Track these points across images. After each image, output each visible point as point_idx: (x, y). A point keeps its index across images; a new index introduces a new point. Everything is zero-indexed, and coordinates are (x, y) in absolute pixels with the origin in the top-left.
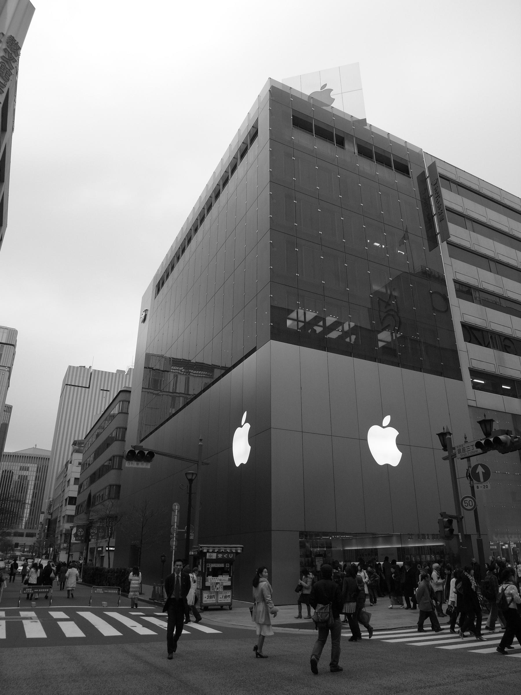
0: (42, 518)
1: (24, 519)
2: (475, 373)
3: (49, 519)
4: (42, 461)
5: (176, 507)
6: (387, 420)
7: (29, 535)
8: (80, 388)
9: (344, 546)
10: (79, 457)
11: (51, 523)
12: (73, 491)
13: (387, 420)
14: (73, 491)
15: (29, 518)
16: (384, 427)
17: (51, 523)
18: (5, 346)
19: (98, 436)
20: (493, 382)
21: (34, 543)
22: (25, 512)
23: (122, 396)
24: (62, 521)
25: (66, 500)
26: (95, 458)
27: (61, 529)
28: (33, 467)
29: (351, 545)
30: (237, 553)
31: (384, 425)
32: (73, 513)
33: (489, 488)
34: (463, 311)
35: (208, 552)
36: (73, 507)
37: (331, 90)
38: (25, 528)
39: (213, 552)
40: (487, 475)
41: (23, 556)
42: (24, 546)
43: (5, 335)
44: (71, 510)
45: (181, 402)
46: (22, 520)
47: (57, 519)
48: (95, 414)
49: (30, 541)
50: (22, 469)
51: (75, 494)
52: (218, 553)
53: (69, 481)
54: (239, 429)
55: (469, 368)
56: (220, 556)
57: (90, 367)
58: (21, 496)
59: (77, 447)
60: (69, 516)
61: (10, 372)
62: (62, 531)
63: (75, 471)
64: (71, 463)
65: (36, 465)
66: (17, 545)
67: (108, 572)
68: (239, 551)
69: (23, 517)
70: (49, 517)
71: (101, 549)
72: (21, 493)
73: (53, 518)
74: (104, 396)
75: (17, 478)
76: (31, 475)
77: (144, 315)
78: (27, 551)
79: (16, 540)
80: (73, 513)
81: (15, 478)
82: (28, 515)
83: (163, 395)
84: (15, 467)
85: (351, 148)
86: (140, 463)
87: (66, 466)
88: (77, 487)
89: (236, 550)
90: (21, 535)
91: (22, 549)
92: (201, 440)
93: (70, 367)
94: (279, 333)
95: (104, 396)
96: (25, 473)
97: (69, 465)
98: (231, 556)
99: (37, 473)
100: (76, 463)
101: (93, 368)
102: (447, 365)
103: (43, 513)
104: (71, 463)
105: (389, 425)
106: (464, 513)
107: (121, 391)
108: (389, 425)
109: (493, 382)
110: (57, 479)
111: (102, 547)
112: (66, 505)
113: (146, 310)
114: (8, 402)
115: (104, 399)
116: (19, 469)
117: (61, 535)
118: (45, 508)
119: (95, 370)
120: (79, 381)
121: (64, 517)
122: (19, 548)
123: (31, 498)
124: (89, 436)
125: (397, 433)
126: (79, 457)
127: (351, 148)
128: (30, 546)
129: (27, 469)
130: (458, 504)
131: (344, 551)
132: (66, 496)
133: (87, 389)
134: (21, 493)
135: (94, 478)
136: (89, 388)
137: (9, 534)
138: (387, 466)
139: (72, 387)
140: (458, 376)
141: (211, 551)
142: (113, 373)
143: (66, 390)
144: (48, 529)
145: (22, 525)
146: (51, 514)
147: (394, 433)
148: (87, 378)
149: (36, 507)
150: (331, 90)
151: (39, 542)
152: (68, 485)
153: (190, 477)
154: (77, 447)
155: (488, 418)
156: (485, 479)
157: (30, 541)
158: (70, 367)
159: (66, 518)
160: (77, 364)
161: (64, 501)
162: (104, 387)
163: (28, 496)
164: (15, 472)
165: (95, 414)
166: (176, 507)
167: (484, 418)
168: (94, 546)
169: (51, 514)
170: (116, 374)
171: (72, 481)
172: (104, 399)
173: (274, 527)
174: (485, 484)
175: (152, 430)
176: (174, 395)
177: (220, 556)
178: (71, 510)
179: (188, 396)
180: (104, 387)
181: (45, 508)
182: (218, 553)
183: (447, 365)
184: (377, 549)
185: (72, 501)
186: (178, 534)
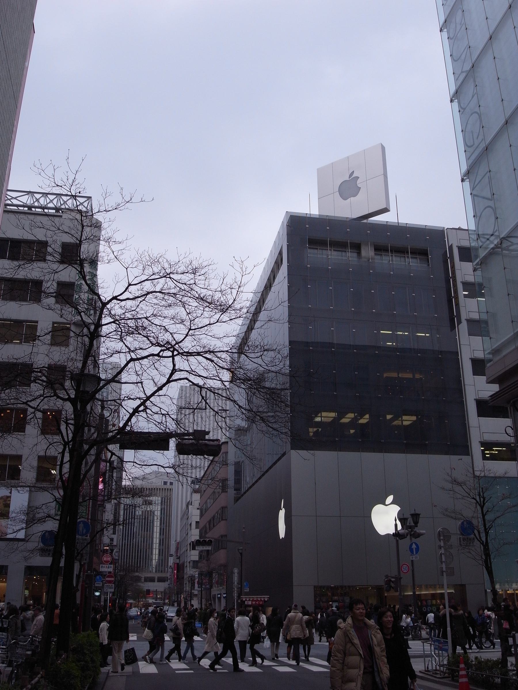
0: (171, 561)
1: (154, 561)
2: (487, 445)
3: (178, 564)
5: (236, 571)
7: (161, 580)
10: (197, 497)
11: (180, 567)
15: (159, 560)
16: (387, 505)
17: (180, 567)
21: (165, 590)
29: (408, 592)
30: (265, 601)
32: (196, 558)
35: (246, 600)
37: (358, 178)
38: (156, 572)
39: (249, 600)
40: (417, 549)
41: (154, 603)
49: (161, 587)
58: (147, 534)
60: (194, 561)
63: (195, 515)
64: (191, 505)
66: (148, 592)
69: (152, 560)
70: (178, 561)
71: (219, 596)
72: (147, 531)
73: (181, 562)
80: (196, 558)
82: (157, 556)
85: (368, 252)
86: (204, 547)
89: (264, 599)
90: (152, 580)
94: (300, 442)
97: (190, 507)
99: (162, 505)
103: (171, 555)
104: (191, 505)
106: (402, 575)
110: (181, 519)
112: (190, 550)
118: (173, 550)
121: (189, 562)
124: (208, 473)
127: (368, 252)
128: (162, 592)
129: (150, 503)
132: (189, 541)
134: (147, 531)
135: (212, 523)
137: (138, 579)
141: (248, 600)
146: (179, 558)
147: (396, 509)
149: (165, 547)
150: (358, 178)
152: (191, 529)
153: (240, 551)
155: (417, 512)
156: (416, 553)
157: (161, 587)
159: (191, 564)
163: (155, 534)
166: (236, 571)
169: (179, 558)
173: (294, 584)
175: (276, 458)
177: (254, 603)
181: (173, 550)
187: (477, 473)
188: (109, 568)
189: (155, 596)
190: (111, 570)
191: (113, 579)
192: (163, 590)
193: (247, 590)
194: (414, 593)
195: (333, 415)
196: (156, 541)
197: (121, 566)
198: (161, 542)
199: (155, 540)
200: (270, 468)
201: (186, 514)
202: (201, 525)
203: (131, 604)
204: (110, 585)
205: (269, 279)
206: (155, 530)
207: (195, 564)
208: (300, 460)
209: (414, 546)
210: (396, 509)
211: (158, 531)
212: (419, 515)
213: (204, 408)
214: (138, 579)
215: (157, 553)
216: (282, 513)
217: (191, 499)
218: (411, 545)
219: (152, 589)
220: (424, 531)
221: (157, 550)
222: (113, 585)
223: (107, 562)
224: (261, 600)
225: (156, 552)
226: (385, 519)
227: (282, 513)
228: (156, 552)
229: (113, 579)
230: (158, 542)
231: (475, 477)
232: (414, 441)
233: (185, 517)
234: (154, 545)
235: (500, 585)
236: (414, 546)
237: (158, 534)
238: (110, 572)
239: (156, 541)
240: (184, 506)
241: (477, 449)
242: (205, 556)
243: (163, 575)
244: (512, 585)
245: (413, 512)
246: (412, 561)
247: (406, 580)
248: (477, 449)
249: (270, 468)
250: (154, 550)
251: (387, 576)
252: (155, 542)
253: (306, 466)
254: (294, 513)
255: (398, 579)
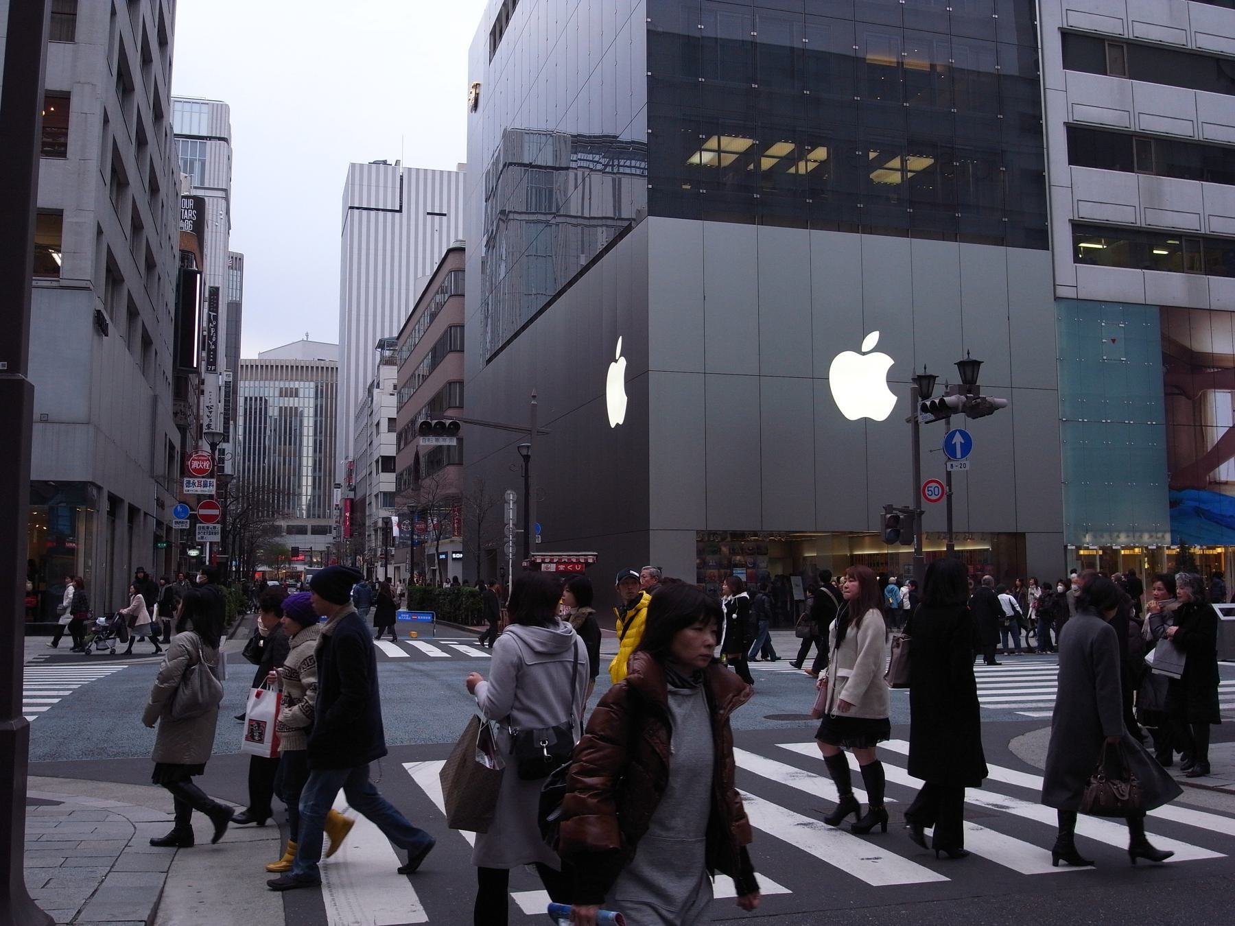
0: (338, 496)
1: (304, 498)
2: (1082, 229)
3: (352, 500)
4: (323, 375)
5: (511, 496)
6: (872, 339)
7: (318, 531)
8: (381, 213)
9: (852, 548)
10: (390, 374)
11: (356, 507)
12: (387, 444)
13: (872, 339)
14: (387, 444)
15: (314, 496)
16: (864, 354)
17: (356, 507)
18: (208, 142)
19: (433, 316)
20: (1131, 245)
22: (304, 483)
23: (451, 263)
24: (374, 504)
25: (377, 462)
26: (434, 365)
27: (373, 520)
28: (307, 389)
29: (862, 547)
30: (587, 563)
31: (864, 349)
32: (391, 488)
33: (968, 467)
34: (1075, 97)
35: (543, 562)
36: (391, 477)
38: (308, 517)
39: (551, 562)
40: (967, 447)
42: (310, 553)
43: (205, 119)
44: (387, 482)
45: (602, 237)
46: (300, 499)
47: (365, 499)
48: (420, 275)
49: (320, 543)
50: (285, 393)
51: (391, 451)
52: (558, 563)
53: (378, 424)
54: (613, 364)
55: (1070, 220)
56: (562, 567)
57: (397, 162)
59: (387, 353)
60: (385, 494)
61: (227, 199)
62: (376, 522)
63: (386, 405)
64: (378, 387)
65: (312, 385)
66: (296, 551)
67: (439, 595)
68: (590, 561)
69: (300, 494)
70: (351, 495)
74: (437, 227)
75: (276, 413)
76: (306, 403)
77: (473, 95)
78: (317, 563)
79: (291, 541)
80: (391, 488)
81: (273, 412)
82: (310, 489)
83: (557, 224)
84: (270, 390)
87: (370, 392)
88: (393, 437)
90: (302, 531)
91: (308, 559)
92: (534, 397)
93: (353, 165)
94: (665, 202)
95: (437, 227)
96: (291, 402)
97: (376, 391)
98: (578, 568)
99: (316, 398)
100: (388, 385)
101: (406, 164)
102: (1021, 220)
103: (338, 486)
104: (378, 387)
105: (877, 349)
106: (925, 505)
107: (450, 251)
108: (877, 349)
109: (1131, 245)
110: (357, 418)
111: (446, 553)
113: (476, 86)
114: (234, 247)
115: (436, 235)
116: (277, 394)
117: (376, 531)
118: (340, 477)
119: (410, 169)
120: (378, 196)
121: (376, 496)
122: (301, 557)
123: (311, 454)
125: (892, 362)
126: (390, 374)
128: (321, 552)
129: (295, 393)
130: (919, 491)
131: (852, 556)
133: (397, 214)
136: (400, 211)
137: (277, 531)
138: (866, 420)
139: (365, 212)
140: (1039, 238)
142: (449, 172)
143: (352, 221)
144: (351, 518)
145: (301, 510)
146: (354, 490)
147: (884, 362)
148: (394, 187)
151: (337, 545)
152: (378, 433)
153: (524, 452)
154: (387, 353)
155: (973, 357)
157: (320, 543)
158: (353, 165)
159: (381, 497)
160: (365, 158)
161: (374, 465)
162: (433, 206)
163: (305, 449)
164: (270, 401)
165: (420, 275)
166: (511, 496)
167: (966, 357)
168: (433, 551)
169: (354, 490)
170: (457, 173)
171: (384, 425)
172: (436, 235)
174: (963, 461)
176: (588, 223)
177: (562, 567)
178: (387, 482)
179: (619, 223)
180: (433, 206)
181: (340, 477)
182: (558, 563)
183: (1021, 220)
184: (898, 554)
185: (387, 464)
186: (516, 536)
187: (1062, 292)
188: (205, 486)
189: (308, 559)
190: (211, 490)
191: (216, 512)
192: (323, 548)
193: (539, 541)
194: (950, 547)
195: (741, 144)
196: (307, 461)
197: (238, 489)
198: (317, 466)
199: (305, 459)
200: (509, 342)
201: (367, 407)
202: (400, 425)
203: (264, 573)
204: (211, 525)
205: (499, 19)
206: (305, 443)
207: (388, 499)
208: (671, 241)
209: (958, 439)
210: (884, 362)
211: (311, 444)
212: (934, 377)
213: (398, 208)
214: (277, 531)
215: (310, 483)
216: (617, 373)
217: (378, 376)
218: (951, 436)
219: (301, 547)
220: (1004, 400)
221: (310, 479)
222: (219, 526)
223: (200, 471)
224: (578, 562)
225: (307, 482)
226: (862, 386)
227: (617, 373)
228: (307, 482)
229: (216, 512)
230: (310, 464)
231: (1057, 299)
232: (928, 213)
233: (366, 411)
234: (304, 469)
235: (1095, 537)
236: (958, 439)
237: (311, 449)
238: (211, 496)
239: (307, 461)
240: (362, 394)
241: (1062, 235)
242: (413, 476)
243: (322, 522)
244: (1141, 537)
245: (921, 372)
246: (949, 474)
247: (933, 518)
248: (1062, 235)
249: (509, 342)
250: (304, 479)
251: (889, 509)
252: (305, 463)
253: (683, 254)
254: (654, 362)
255: (914, 516)
